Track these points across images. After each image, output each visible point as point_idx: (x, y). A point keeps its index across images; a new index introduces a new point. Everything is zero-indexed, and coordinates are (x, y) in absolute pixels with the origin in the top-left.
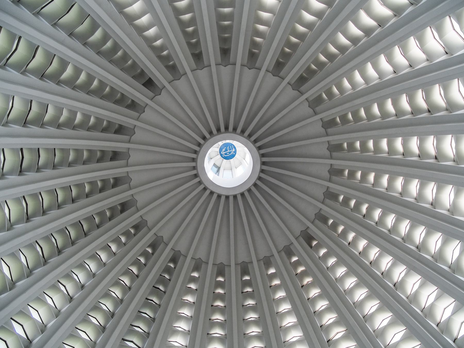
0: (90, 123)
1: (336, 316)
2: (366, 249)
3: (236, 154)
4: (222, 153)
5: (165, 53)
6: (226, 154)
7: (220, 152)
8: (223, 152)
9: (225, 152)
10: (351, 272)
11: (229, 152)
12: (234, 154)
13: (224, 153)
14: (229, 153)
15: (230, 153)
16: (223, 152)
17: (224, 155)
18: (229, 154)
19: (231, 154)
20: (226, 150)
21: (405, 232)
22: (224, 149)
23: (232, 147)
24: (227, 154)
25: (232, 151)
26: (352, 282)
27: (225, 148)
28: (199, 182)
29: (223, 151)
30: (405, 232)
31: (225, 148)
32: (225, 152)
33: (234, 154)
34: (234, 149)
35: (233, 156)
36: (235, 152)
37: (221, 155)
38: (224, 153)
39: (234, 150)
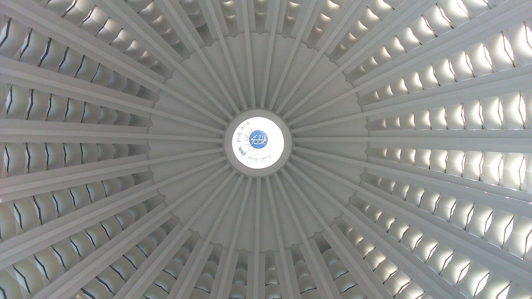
0: (352, 35)
1: (468, 262)
2: (432, 25)
3: (266, 144)
4: (252, 140)
5: (145, 54)
6: (256, 142)
7: (250, 138)
8: (253, 139)
9: (255, 140)
10: (435, 149)
11: (259, 141)
12: (264, 144)
13: (254, 140)
14: (259, 142)
15: (260, 142)
16: (253, 139)
17: (253, 142)
18: (258, 143)
19: (261, 143)
20: (257, 138)
21: (429, 256)
22: (255, 136)
23: (264, 136)
24: (257, 142)
25: (263, 141)
26: (446, 259)
27: (257, 135)
28: (230, 168)
29: (254, 138)
30: (429, 256)
31: (257, 135)
32: (255, 140)
33: (264, 144)
34: (265, 139)
35: (262, 146)
36: (266, 143)
37: (251, 141)
38: (254, 140)
39: (265, 140)
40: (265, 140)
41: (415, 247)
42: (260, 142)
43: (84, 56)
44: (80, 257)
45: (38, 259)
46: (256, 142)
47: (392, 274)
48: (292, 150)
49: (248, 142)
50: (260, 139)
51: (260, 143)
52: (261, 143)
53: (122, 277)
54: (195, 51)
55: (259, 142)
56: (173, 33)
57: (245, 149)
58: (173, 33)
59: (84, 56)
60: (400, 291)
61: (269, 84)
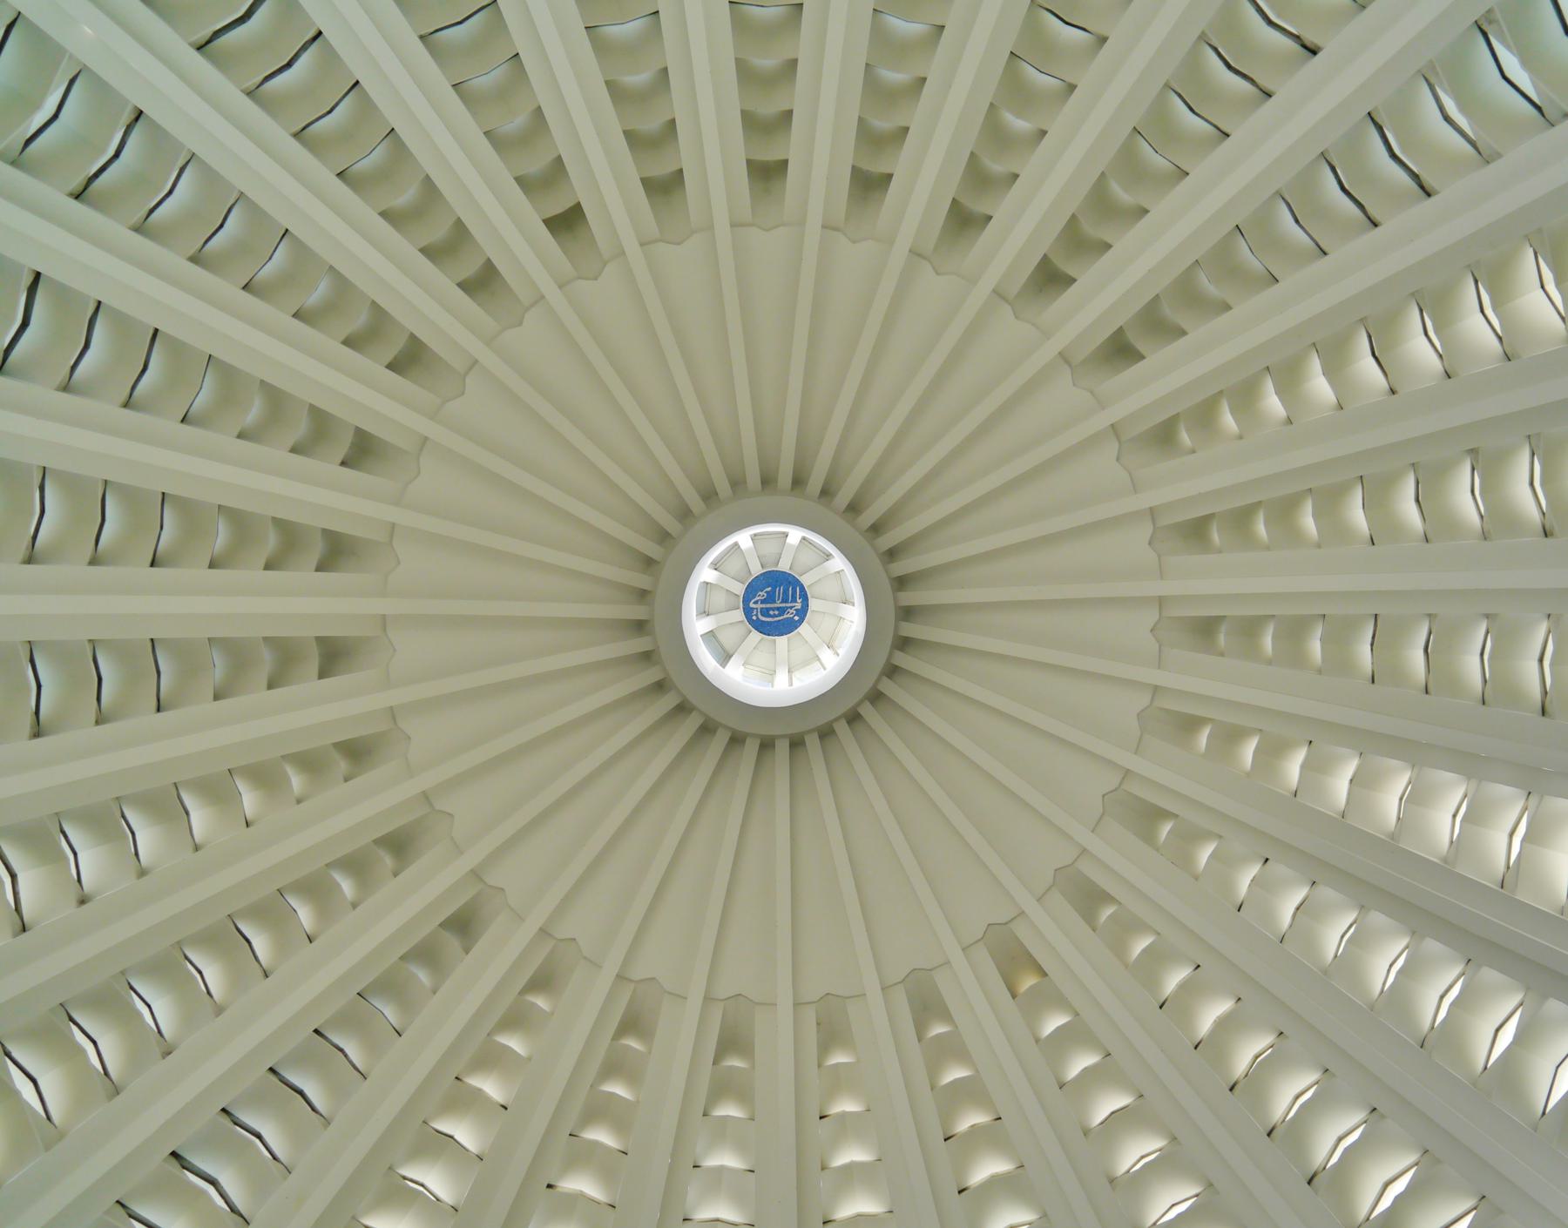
4: (752, 605)
6: (765, 612)
7: (746, 600)
9: (764, 606)
11: (778, 609)
12: (796, 618)
13: (759, 606)
14: (777, 612)
15: (782, 611)
16: (756, 603)
17: (757, 615)
18: (775, 616)
19: (785, 616)
20: (770, 598)
24: (771, 613)
25: (791, 608)
27: (769, 589)
31: (769, 589)
32: (764, 606)
33: (796, 618)
37: (748, 612)
38: (759, 606)
40: (798, 606)
41: (1336, 956)
42: (782, 611)
43: (156, 331)
44: (1207, 40)
45: (15, 1055)
46: (765, 612)
47: (1264, 1053)
48: (894, 636)
49: (739, 615)
50: (781, 603)
51: (780, 615)
52: (785, 616)
53: (313, 1109)
54: (1162, 574)
55: (777, 612)
56: (1250, 650)
57: (727, 639)
58: (1250, 650)
59: (156, 331)
60: (1290, 1109)
61: (940, 739)
